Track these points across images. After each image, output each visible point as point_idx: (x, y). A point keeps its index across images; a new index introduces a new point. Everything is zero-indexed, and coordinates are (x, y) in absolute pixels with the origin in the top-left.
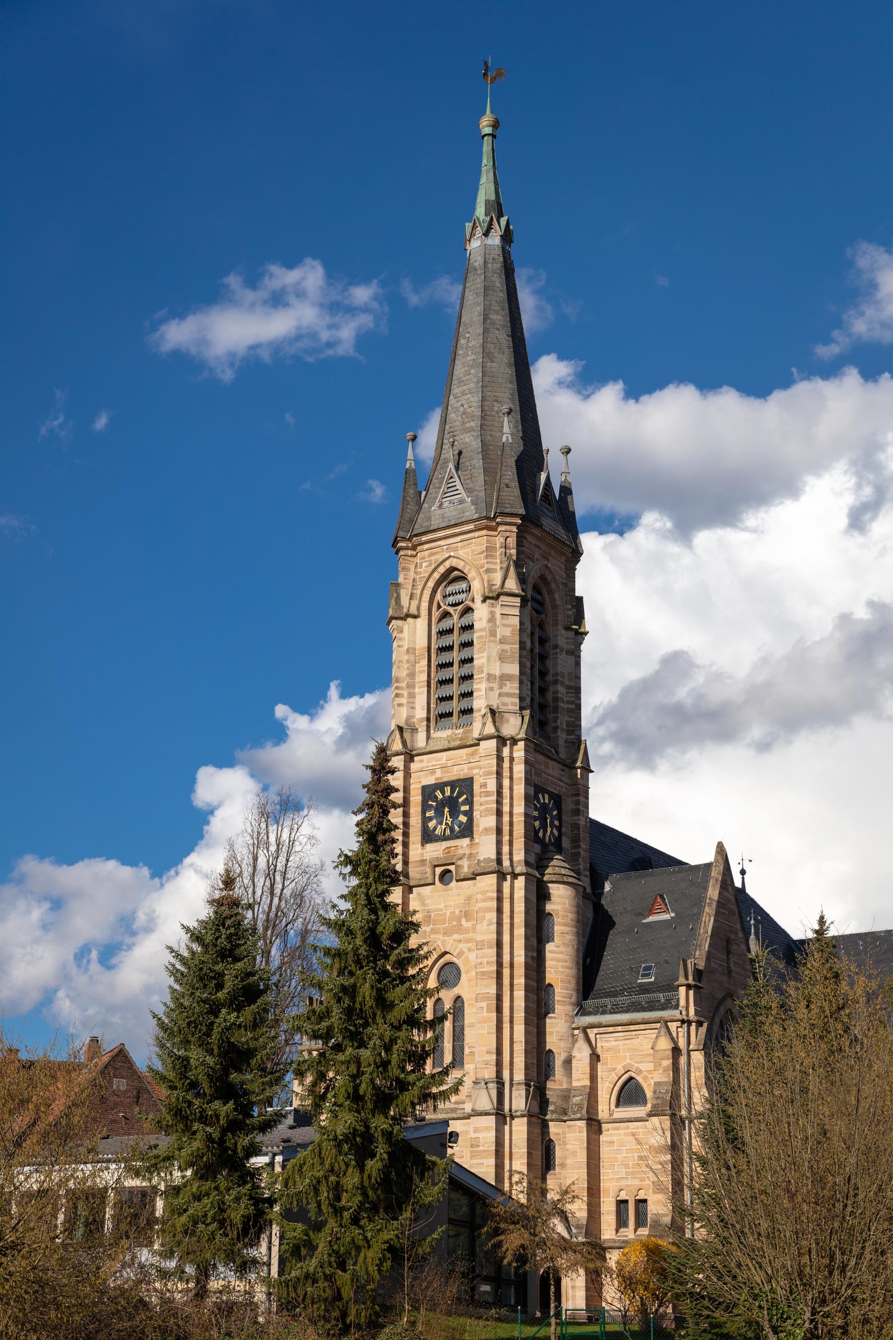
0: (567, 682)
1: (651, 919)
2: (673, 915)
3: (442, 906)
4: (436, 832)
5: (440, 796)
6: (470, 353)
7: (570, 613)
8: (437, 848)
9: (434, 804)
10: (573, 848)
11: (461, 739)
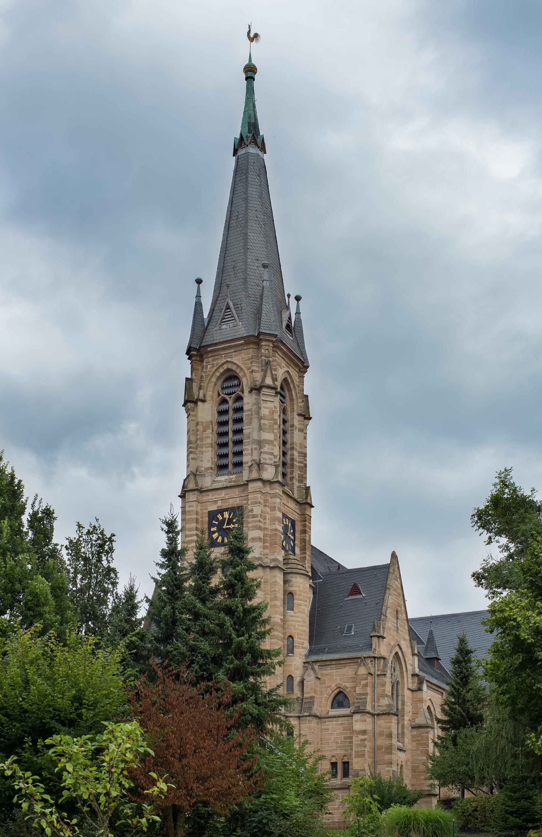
4: (218, 541)
5: (220, 518)
6: (239, 226)
9: (216, 523)
11: (234, 481)
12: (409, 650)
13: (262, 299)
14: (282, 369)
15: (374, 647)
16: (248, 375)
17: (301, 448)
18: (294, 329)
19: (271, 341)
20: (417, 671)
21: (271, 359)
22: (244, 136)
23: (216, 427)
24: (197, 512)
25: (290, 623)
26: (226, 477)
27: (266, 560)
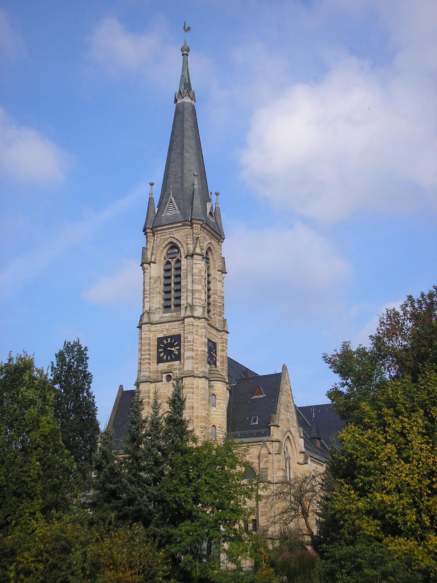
0: (218, 294)
1: (255, 397)
2: (264, 395)
3: (166, 391)
5: (166, 343)
6: (178, 148)
7: (220, 264)
8: (165, 365)
10: (221, 366)
12: (298, 434)
13: (193, 196)
14: (206, 241)
15: (272, 433)
16: (185, 246)
17: (220, 293)
18: (215, 214)
19: (200, 224)
20: (304, 449)
21: (199, 236)
22: (182, 91)
23: (163, 280)
24: (149, 338)
25: (214, 416)
26: (170, 314)
27: (196, 372)
